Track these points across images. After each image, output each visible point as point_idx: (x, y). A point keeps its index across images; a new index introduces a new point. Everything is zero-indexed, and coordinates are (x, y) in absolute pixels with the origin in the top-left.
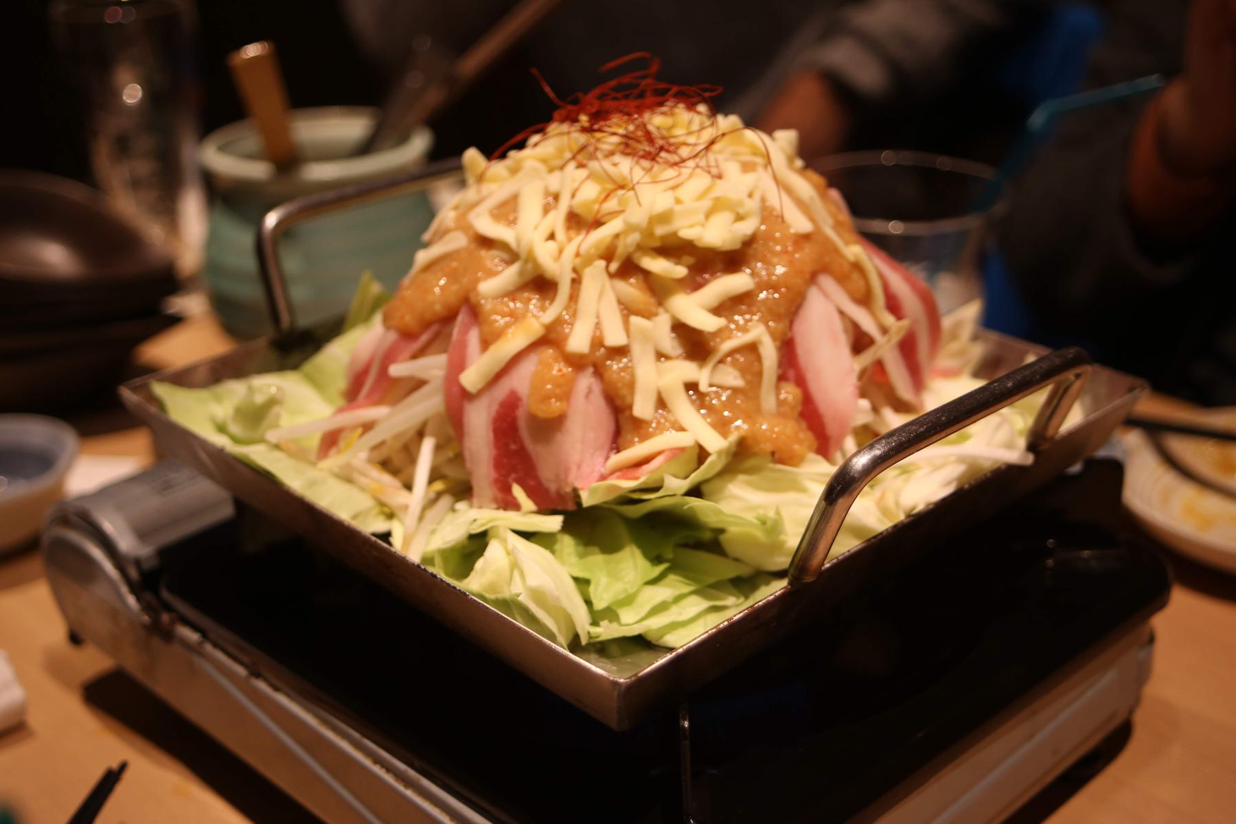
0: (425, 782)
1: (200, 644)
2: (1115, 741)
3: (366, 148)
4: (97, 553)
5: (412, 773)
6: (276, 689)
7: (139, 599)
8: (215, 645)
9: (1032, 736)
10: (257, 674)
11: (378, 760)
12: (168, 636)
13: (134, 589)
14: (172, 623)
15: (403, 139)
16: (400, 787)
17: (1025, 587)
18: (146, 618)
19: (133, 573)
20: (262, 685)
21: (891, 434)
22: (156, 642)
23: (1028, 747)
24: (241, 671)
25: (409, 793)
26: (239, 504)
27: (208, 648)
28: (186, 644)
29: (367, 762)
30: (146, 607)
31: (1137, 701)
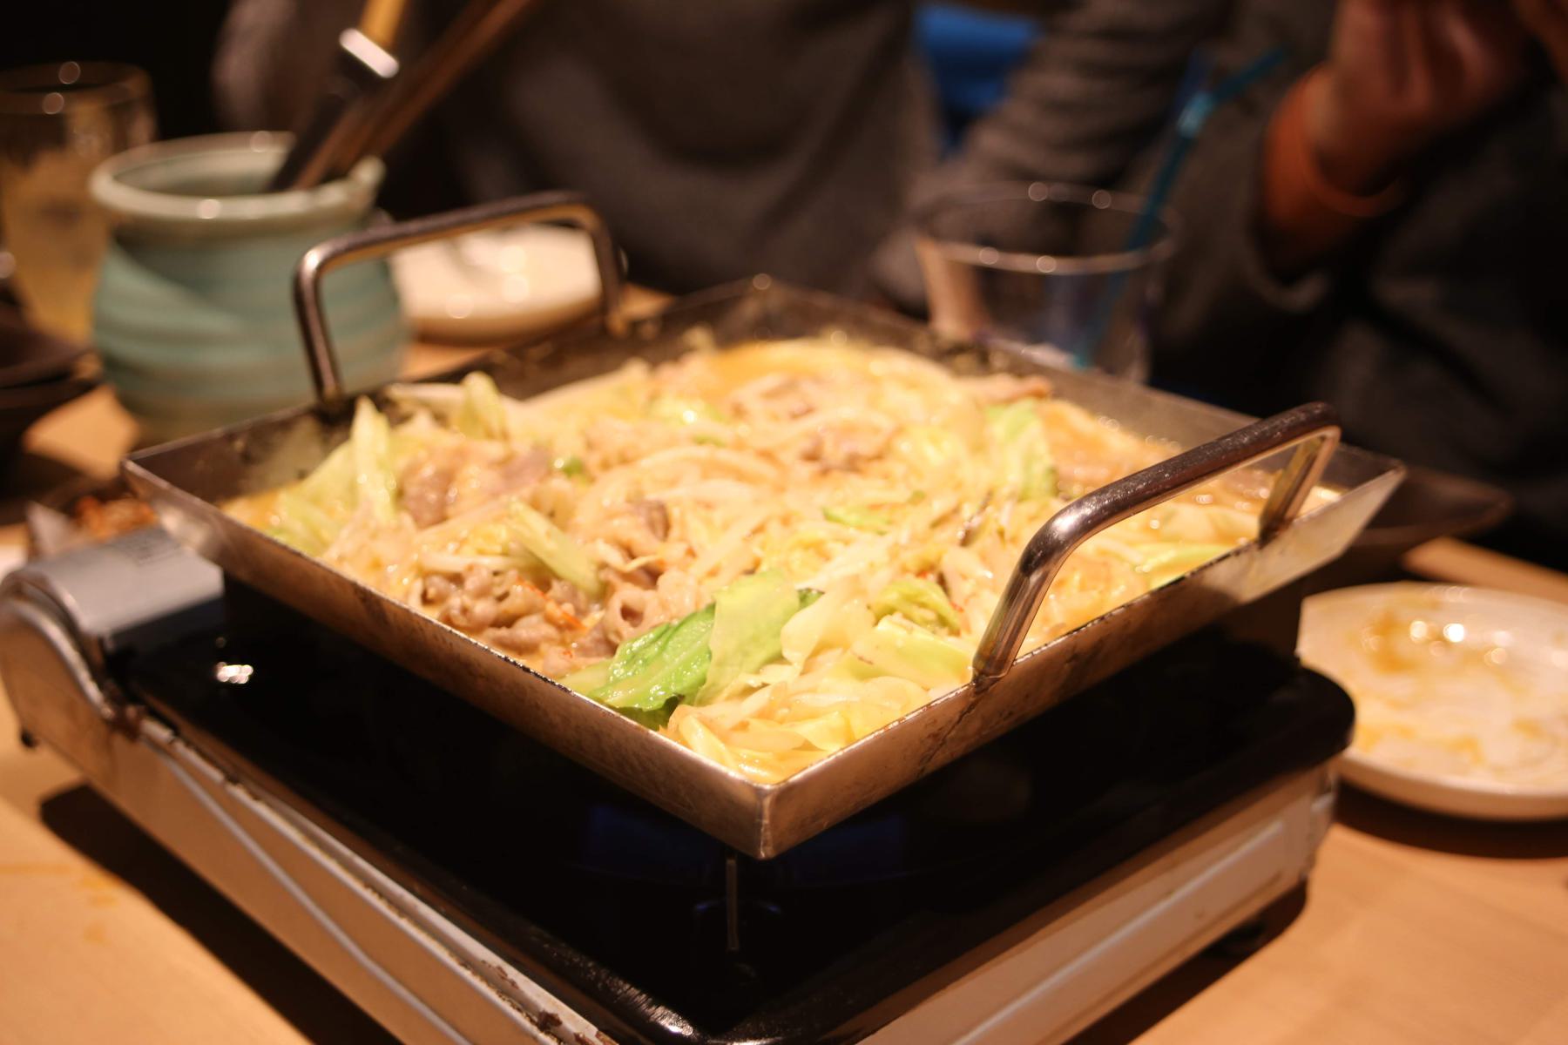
0: (425, 910)
1: (171, 743)
2: (1287, 908)
3: (282, 181)
4: (55, 632)
5: (409, 898)
6: (256, 798)
7: (101, 687)
8: (188, 744)
9: (1169, 893)
10: (233, 779)
11: (370, 884)
12: (131, 732)
13: (96, 676)
14: (139, 717)
15: (336, 173)
16: (392, 915)
17: (1164, 736)
18: (108, 711)
19: (97, 656)
20: (239, 793)
21: (200, 517)
22: (119, 741)
23: (1163, 906)
24: (216, 776)
25: (404, 924)
26: (229, 580)
27: (180, 747)
28: (155, 744)
29: (357, 886)
30: (111, 698)
31: (1311, 861)
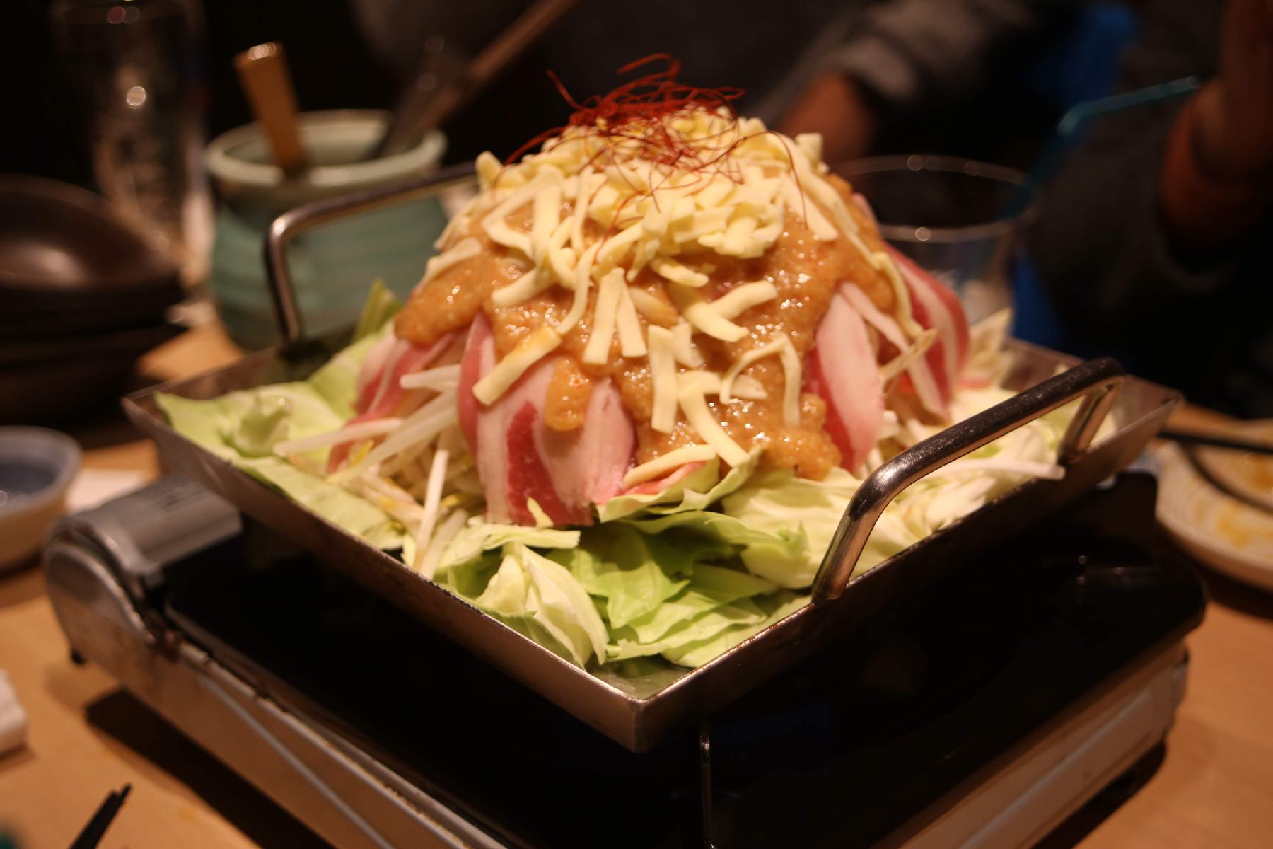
0: (438, 806)
1: (206, 663)
2: (1148, 764)
3: (377, 152)
4: (100, 570)
5: (424, 796)
6: (285, 710)
7: (143, 617)
8: (222, 665)
9: (1062, 758)
10: (264, 695)
11: (389, 784)
12: (173, 655)
13: (138, 607)
14: (178, 642)
15: (415, 143)
16: (412, 811)
17: (1056, 605)
18: (150, 637)
19: (137, 591)
20: (269, 706)
21: (918, 447)
22: (161, 661)
23: (1058, 770)
24: (248, 691)
25: (421, 817)
26: (246, 519)
27: (215, 667)
28: (192, 664)
29: (378, 786)
30: (151, 626)
31: (1171, 722)
